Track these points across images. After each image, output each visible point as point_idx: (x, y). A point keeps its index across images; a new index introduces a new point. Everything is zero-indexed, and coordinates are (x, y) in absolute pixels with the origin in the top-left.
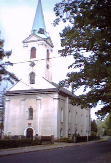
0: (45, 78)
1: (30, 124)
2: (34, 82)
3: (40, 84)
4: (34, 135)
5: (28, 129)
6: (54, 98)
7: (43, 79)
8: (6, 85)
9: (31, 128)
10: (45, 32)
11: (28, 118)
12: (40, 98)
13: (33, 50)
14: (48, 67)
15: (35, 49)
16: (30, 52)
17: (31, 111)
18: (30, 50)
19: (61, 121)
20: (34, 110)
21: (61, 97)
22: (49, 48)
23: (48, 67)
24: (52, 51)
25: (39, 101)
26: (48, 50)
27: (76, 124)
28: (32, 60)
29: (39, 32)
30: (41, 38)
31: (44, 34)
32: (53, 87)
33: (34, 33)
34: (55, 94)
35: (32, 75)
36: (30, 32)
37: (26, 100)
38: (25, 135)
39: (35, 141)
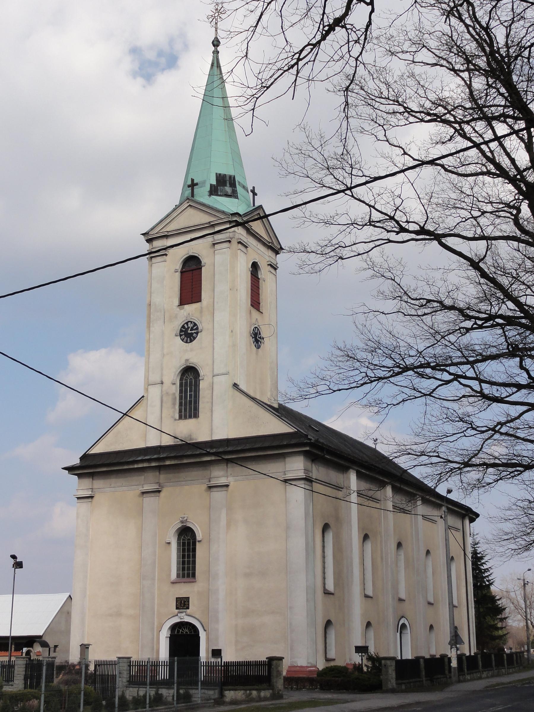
0: (242, 387)
1: (183, 603)
2: (196, 409)
3: (222, 420)
4: (204, 654)
5: (174, 627)
6: (289, 476)
7: (237, 393)
8: (355, 1)
9: (187, 619)
10: (239, 189)
11: (174, 575)
12: (223, 481)
13: (192, 268)
14: (257, 338)
15: (200, 262)
16: (178, 275)
17: (187, 538)
18: (179, 266)
19: (324, 587)
20: (199, 538)
21: (319, 472)
22: (263, 256)
23: (257, 338)
24: (274, 267)
25: (218, 495)
26: (255, 266)
27: (401, 600)
28: (190, 309)
29: (214, 191)
30: (223, 212)
31: (234, 195)
32: (278, 427)
33: (193, 195)
34: (288, 460)
35: (190, 375)
36: (174, 194)
37: (162, 494)
38: (164, 654)
39: (494, 638)
